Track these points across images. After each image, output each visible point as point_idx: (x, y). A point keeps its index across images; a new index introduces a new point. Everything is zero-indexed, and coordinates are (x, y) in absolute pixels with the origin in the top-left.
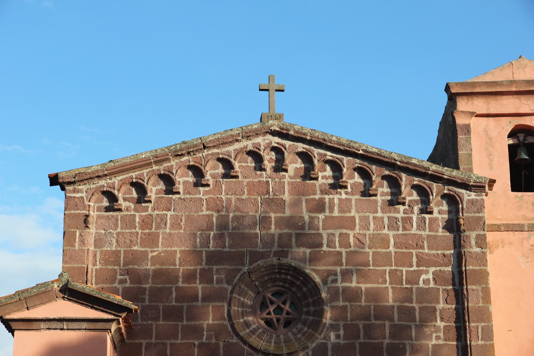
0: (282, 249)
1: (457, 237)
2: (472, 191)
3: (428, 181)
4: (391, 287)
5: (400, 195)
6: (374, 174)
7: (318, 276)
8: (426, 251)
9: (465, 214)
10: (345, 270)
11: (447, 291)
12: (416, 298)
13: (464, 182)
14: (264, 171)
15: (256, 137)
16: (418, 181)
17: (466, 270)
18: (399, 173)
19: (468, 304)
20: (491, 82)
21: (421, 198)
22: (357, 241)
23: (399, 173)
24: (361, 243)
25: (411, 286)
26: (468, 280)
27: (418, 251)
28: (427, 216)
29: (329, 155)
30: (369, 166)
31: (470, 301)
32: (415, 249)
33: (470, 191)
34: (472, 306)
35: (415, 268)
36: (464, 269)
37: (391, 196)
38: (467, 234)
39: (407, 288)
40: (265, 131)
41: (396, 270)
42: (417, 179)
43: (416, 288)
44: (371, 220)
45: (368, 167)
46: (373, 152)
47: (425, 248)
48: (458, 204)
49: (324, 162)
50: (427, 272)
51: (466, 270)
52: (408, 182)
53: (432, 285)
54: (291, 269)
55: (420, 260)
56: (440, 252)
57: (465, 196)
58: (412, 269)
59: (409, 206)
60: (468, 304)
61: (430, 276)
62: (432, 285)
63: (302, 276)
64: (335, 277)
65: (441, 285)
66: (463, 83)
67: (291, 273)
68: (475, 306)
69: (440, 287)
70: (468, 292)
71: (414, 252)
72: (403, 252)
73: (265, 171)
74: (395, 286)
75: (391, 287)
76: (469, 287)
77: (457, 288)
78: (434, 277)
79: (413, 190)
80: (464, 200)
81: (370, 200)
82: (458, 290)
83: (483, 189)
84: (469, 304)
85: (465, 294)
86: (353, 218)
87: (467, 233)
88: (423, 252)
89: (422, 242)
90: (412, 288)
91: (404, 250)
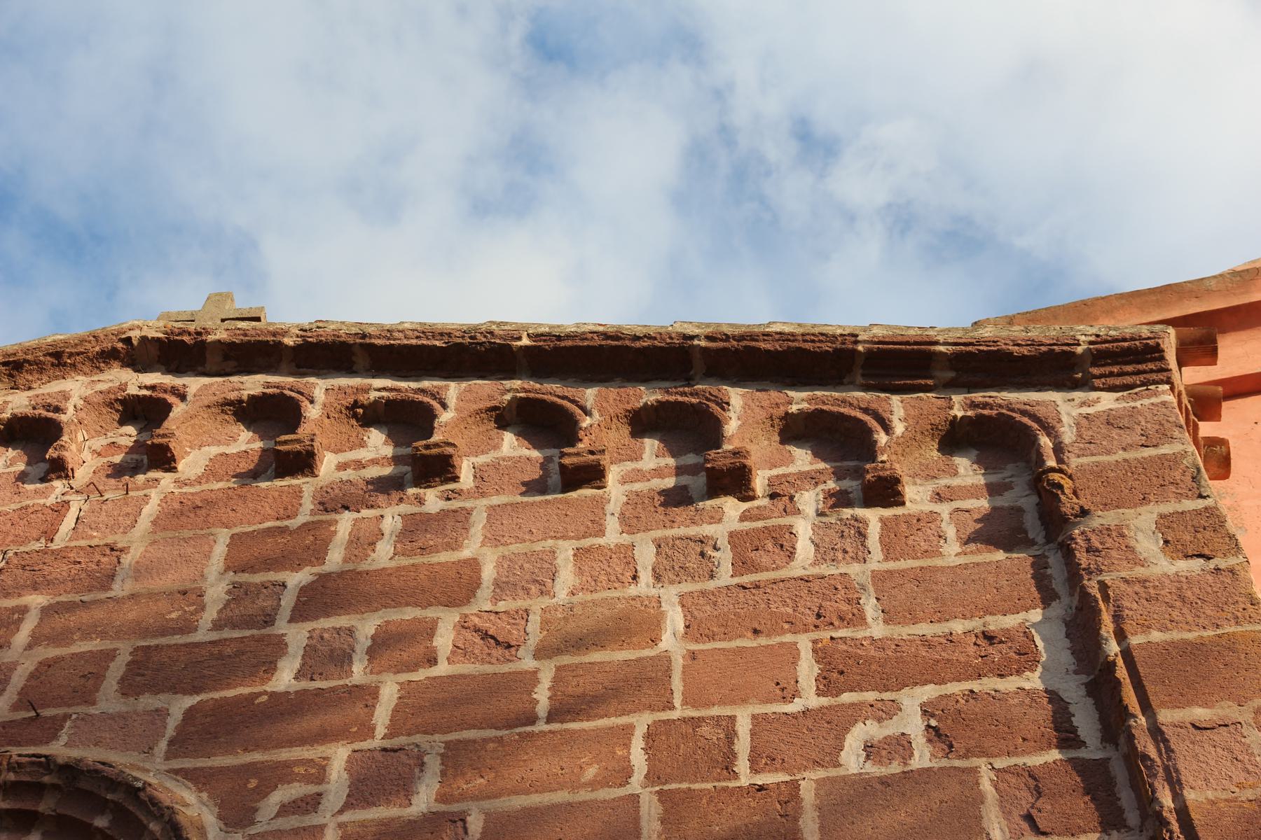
0: (33, 714)
1: (1055, 561)
2: (1097, 382)
3: (862, 394)
4: (659, 793)
5: (718, 445)
6: (587, 413)
7: (205, 795)
8: (878, 629)
9: (1074, 462)
10: (378, 756)
11: (1035, 780)
12: (822, 828)
13: (1043, 349)
14: (59, 477)
15: (56, 378)
16: (809, 401)
17: (1127, 654)
18: (714, 390)
19: (1177, 796)
20: (1152, 291)
21: (834, 464)
22: (478, 640)
23: (714, 390)
24: (498, 643)
25: (787, 778)
26: (1150, 688)
27: (825, 635)
28: (873, 517)
29: (379, 387)
30: (570, 392)
31: (1186, 776)
32: (806, 631)
33: (1084, 384)
34: (1213, 803)
35: (810, 699)
36: (1113, 648)
37: (677, 475)
38: (1101, 521)
39: (761, 788)
40: (97, 349)
41: (696, 722)
42: (804, 395)
43: (816, 781)
44: (567, 560)
45: (564, 398)
46: (584, 333)
47: (869, 620)
48: (1033, 441)
49: (355, 416)
50: (888, 711)
51: (1127, 654)
52: (757, 410)
53: (923, 757)
54: (46, 779)
55: (841, 667)
56: (958, 627)
57: (1064, 408)
58: (795, 707)
59: (773, 496)
60: (1177, 796)
61: (913, 725)
62: (923, 757)
63: (102, 806)
64: (312, 789)
65: (984, 753)
66: (1036, 312)
67: (45, 806)
68: (1235, 800)
69: (981, 763)
70: (1166, 741)
71: (804, 643)
72: (740, 651)
73: (67, 477)
74: (684, 786)
75: (659, 793)
76: (1166, 716)
77: (1093, 750)
78: (933, 723)
79: (788, 447)
80: (1060, 421)
81: (567, 502)
82: (1104, 763)
83: (1151, 366)
84: (1190, 796)
85: (1145, 757)
86: (474, 565)
87: (1103, 518)
88: (860, 634)
89: (849, 601)
90: (794, 785)
91: (748, 642)
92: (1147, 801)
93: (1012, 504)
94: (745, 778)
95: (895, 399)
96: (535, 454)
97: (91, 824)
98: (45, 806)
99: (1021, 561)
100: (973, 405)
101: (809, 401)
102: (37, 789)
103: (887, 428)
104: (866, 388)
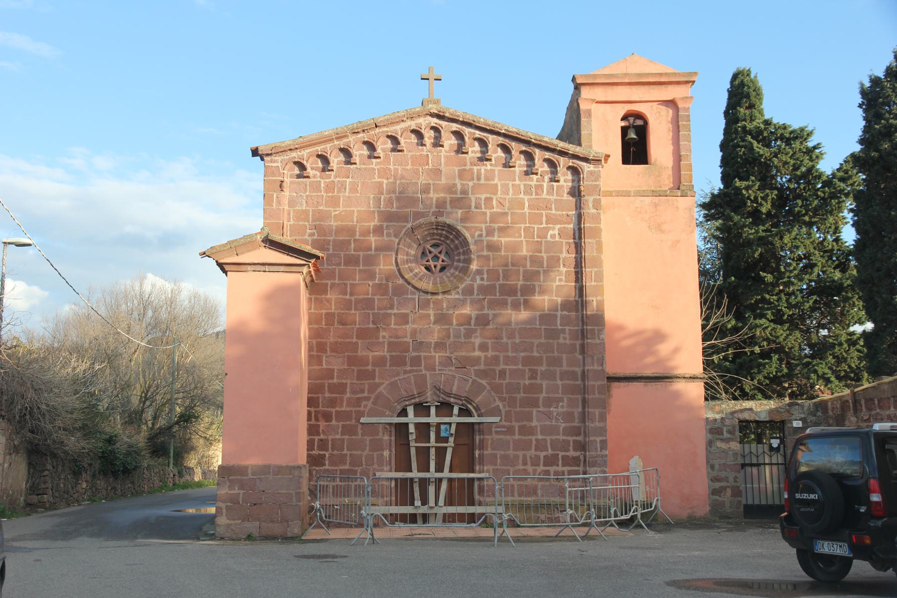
8: (554, 212)
9: (585, 183)
30: (510, 142)
33: (590, 163)
35: (544, 225)
36: (583, 226)
50: (554, 229)
58: (542, 226)
62: (557, 239)
67: (445, 229)
71: (544, 212)
76: (586, 240)
77: (577, 241)
87: (586, 198)
92: (581, 253)
93: (566, 299)
94: (536, 240)
95: (562, 158)
96: (503, 155)
97: (883, 501)
98: (445, 229)
99: (573, 200)
100: (573, 163)
101: (549, 155)
102: (445, 226)
103: (560, 166)
104: (557, 155)
